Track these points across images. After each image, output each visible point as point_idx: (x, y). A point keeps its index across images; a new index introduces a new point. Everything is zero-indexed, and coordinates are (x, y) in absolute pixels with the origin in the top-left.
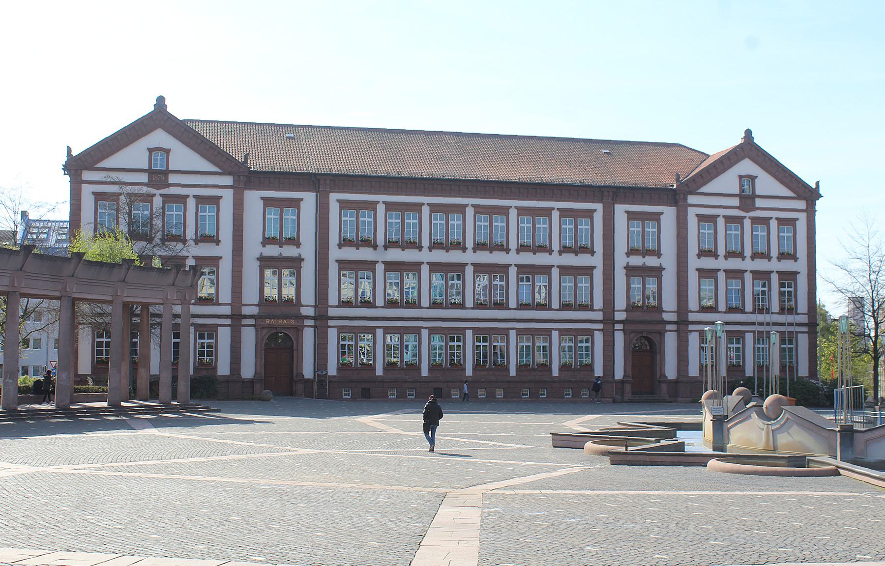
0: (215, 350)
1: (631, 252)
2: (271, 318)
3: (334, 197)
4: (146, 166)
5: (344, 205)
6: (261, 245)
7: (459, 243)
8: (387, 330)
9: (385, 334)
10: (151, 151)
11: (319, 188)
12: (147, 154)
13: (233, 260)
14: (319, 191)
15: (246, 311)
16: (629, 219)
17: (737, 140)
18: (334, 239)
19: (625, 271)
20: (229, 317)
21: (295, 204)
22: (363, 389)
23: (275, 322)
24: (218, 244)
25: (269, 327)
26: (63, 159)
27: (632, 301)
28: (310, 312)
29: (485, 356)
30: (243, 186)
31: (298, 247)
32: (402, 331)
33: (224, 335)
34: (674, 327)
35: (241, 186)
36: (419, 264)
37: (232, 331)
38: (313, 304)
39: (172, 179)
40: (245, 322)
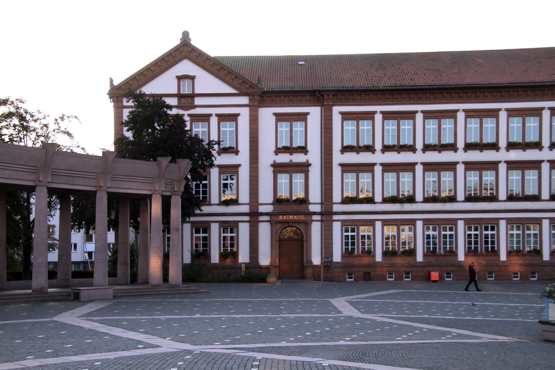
0: (209, 243)
1: (278, 151)
2: (283, 215)
3: (337, 110)
4: (176, 92)
5: (346, 116)
6: (274, 154)
7: (233, 148)
8: (385, 223)
9: (383, 225)
10: (179, 78)
11: (323, 102)
12: (176, 81)
13: (251, 167)
14: (323, 106)
15: (262, 209)
16: (277, 120)
17: (176, 42)
18: (337, 146)
19: (272, 169)
20: (248, 214)
21: (303, 117)
22: (365, 273)
23: (287, 217)
24: (237, 154)
25: (282, 222)
26: (108, 88)
27: (279, 195)
28: (316, 208)
29: (476, 243)
30: (257, 104)
31: (306, 154)
32: (398, 223)
33: (244, 230)
34: (318, 217)
35: (330, 104)
36: (455, 164)
37: (251, 226)
38: (319, 201)
39: (198, 101)
40: (261, 218)
